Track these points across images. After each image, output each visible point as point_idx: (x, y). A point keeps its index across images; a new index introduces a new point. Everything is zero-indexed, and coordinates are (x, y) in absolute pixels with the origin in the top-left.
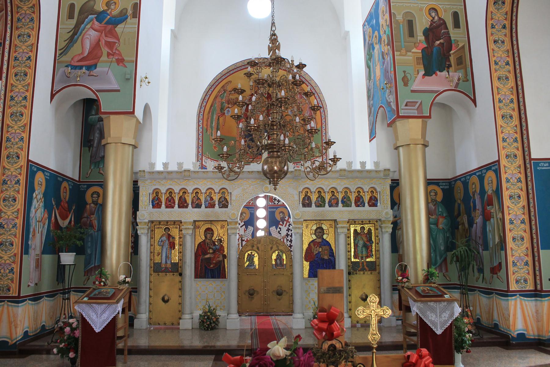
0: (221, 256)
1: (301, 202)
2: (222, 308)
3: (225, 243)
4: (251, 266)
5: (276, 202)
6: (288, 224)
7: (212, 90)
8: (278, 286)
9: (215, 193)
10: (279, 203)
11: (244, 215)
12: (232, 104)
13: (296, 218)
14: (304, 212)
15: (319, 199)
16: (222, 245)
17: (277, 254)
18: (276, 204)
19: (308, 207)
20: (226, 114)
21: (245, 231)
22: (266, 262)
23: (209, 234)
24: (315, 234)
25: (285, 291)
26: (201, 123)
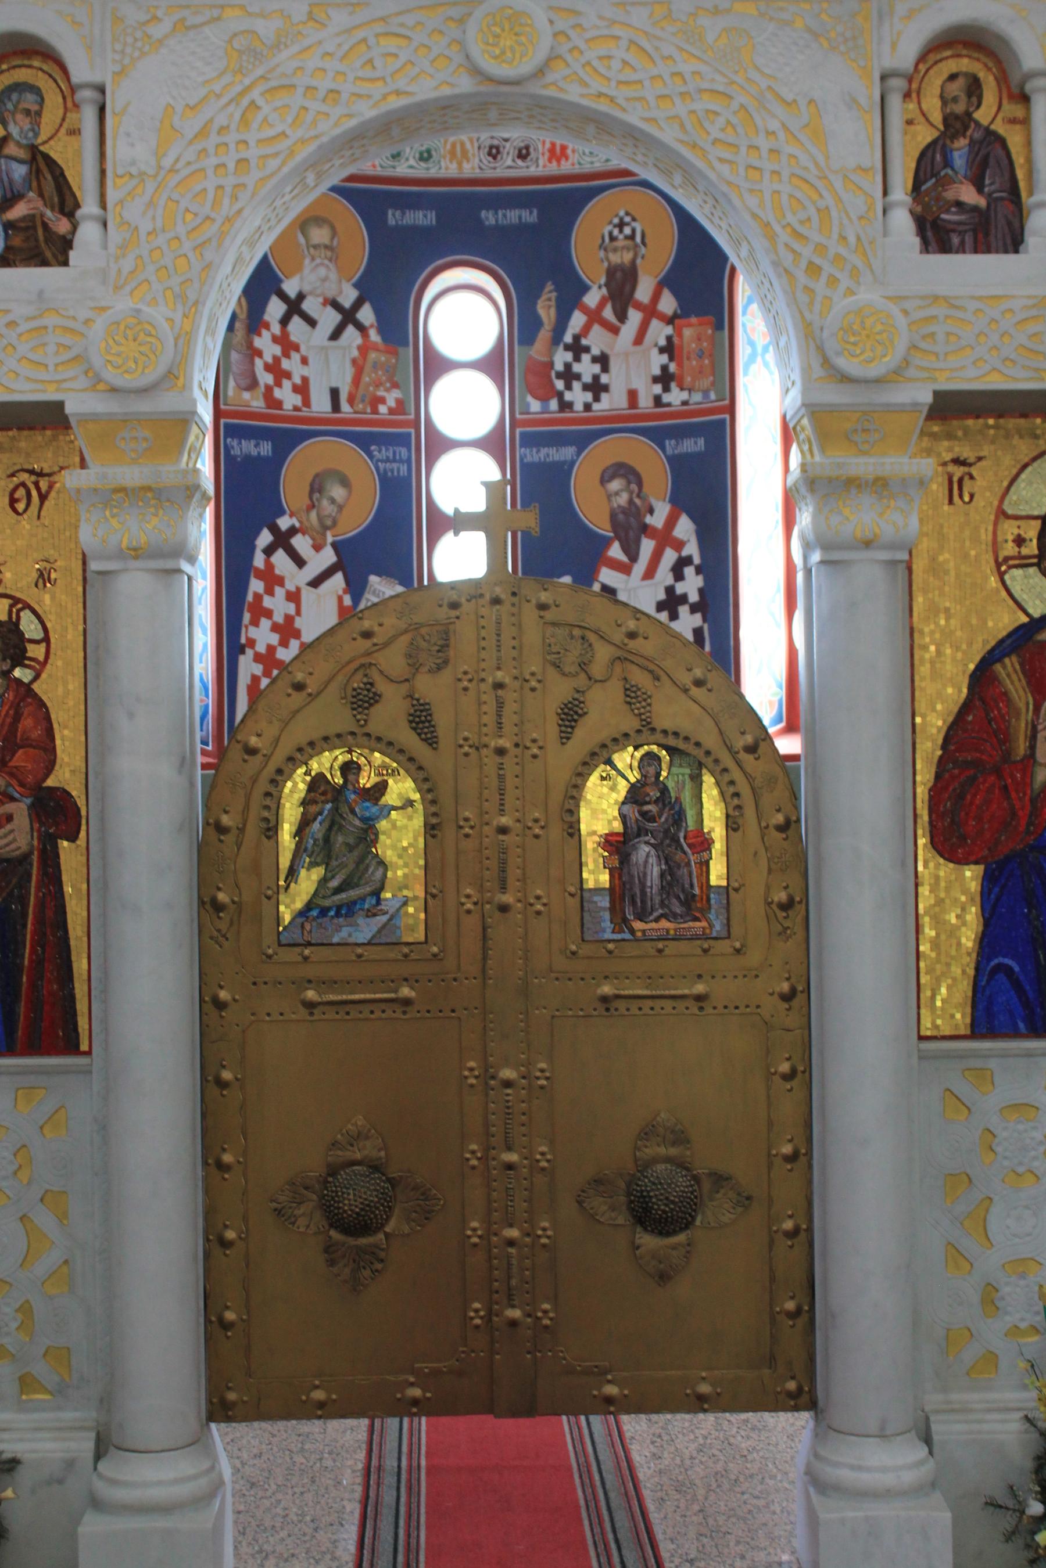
0: (20, 810)
1: (901, 193)
2: (40, 1369)
3: (56, 663)
4: (347, 911)
5: (578, 396)
6: (670, 557)
8: (648, 1132)
10: (597, 399)
11: (338, 492)
16: (26, 691)
17: (633, 776)
18: (579, 407)
19: (976, 251)
22: (513, 874)
25: (720, 1179)
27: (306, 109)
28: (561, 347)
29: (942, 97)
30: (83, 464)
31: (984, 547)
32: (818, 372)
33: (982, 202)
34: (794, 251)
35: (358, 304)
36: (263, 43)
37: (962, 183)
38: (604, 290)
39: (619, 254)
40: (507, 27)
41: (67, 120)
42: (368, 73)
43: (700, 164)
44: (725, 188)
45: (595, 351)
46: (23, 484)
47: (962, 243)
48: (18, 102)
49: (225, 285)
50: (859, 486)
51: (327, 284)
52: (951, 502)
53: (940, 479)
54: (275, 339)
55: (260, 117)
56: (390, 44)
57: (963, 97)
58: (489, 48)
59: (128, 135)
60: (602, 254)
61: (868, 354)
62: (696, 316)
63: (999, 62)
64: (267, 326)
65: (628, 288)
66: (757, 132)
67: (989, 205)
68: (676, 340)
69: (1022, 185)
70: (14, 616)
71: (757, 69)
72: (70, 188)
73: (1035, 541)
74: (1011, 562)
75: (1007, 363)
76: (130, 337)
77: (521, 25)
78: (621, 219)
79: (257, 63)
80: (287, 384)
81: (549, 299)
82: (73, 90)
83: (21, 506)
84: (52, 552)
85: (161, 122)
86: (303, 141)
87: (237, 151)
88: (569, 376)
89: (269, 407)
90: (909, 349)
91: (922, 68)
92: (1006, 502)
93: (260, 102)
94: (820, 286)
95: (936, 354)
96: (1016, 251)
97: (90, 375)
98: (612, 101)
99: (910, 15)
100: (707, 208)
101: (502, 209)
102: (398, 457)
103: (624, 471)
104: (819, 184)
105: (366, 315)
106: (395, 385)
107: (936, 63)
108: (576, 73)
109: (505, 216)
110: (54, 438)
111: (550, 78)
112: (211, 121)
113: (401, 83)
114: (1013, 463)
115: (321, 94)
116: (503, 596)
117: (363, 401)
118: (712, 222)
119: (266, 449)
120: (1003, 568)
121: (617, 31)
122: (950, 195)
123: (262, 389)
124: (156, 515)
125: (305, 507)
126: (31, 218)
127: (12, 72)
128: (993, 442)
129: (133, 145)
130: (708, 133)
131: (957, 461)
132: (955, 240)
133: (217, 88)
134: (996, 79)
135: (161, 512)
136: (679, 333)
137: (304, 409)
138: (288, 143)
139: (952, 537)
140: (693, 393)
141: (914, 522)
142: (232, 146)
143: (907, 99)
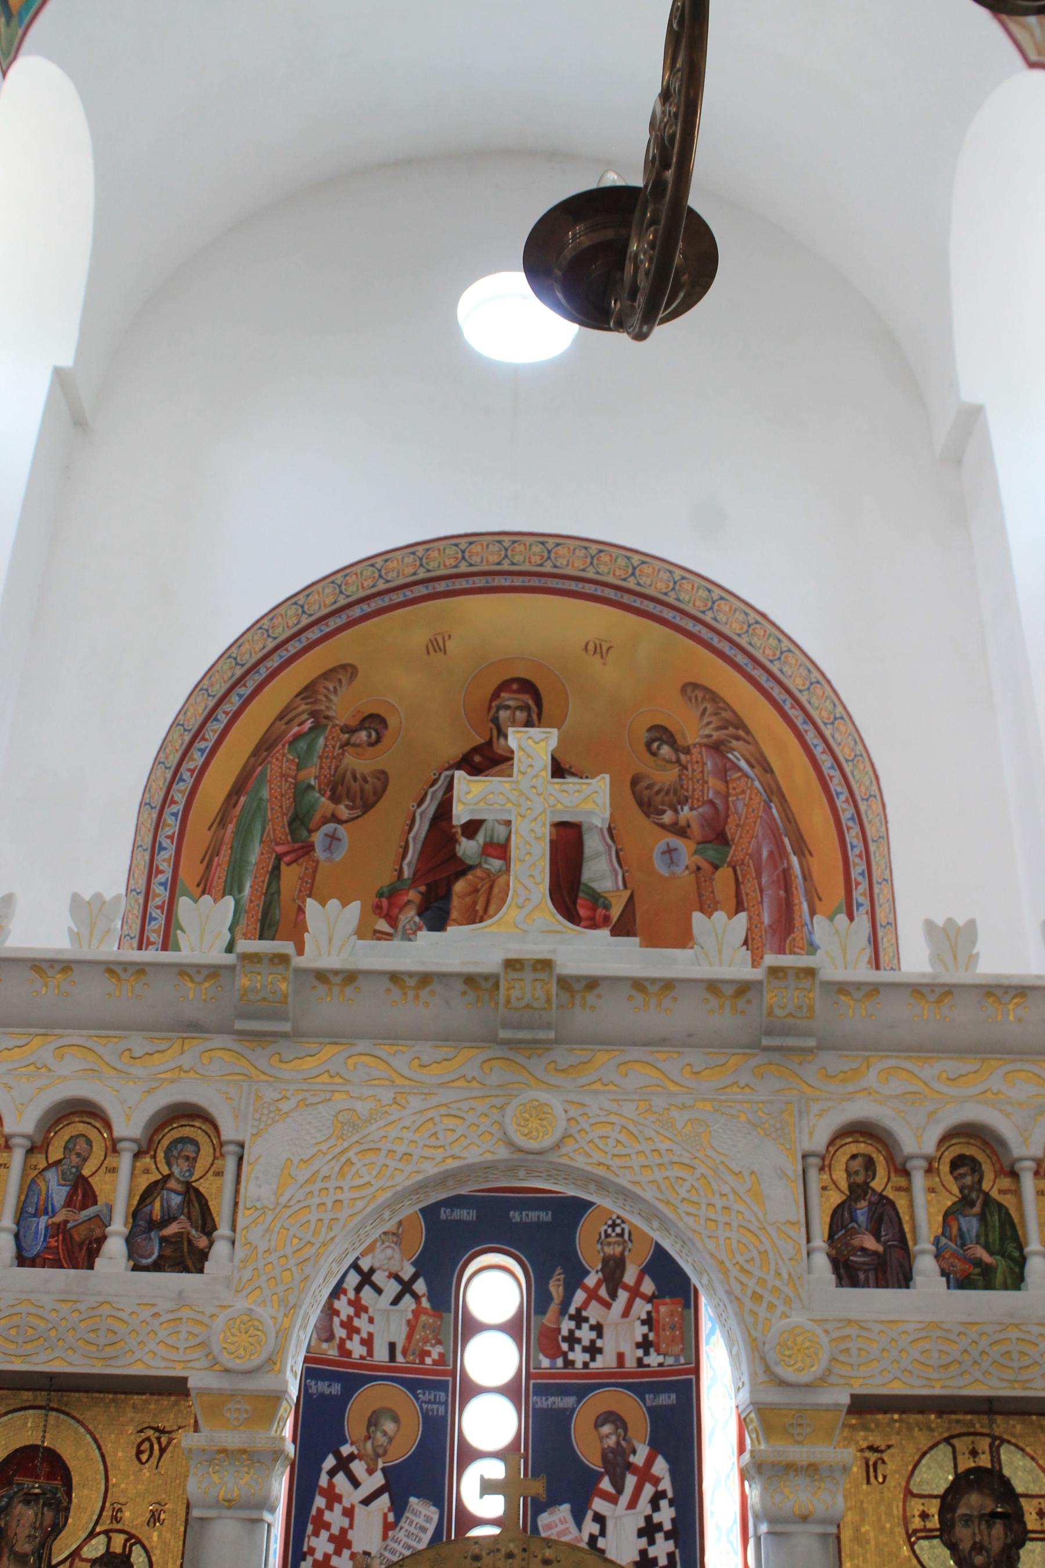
1: (820, 1241)
5: (579, 1356)
6: (648, 1490)
7: (245, 691)
9: (113, 1147)
10: (593, 1359)
11: (389, 1426)
12: (353, 800)
13: (786, 1373)
14: (852, 1331)
15: (971, 1224)
18: (579, 1364)
19: (877, 1286)
20: (319, 853)
21: (388, 1527)
23: (29, 1499)
24: (946, 1533)
26: (165, 855)
27: (387, 1166)
28: (567, 1317)
29: (847, 1171)
30: (196, 1430)
31: (896, 1520)
32: (762, 1377)
33: (880, 1249)
34: (742, 1283)
35: (414, 1278)
36: (360, 1118)
37: (864, 1234)
38: (600, 1275)
39: (612, 1247)
40: (534, 1114)
41: (214, 1166)
42: (432, 1142)
43: (671, 1216)
44: (690, 1234)
45: (593, 1321)
46: (148, 1439)
47: (867, 1279)
48: (182, 1150)
49: (317, 1292)
50: (796, 1470)
51: (392, 1261)
52: (868, 1482)
53: (859, 1463)
54: (350, 1303)
55: (354, 1169)
56: (450, 1122)
57: (862, 1173)
58: (522, 1129)
59: (257, 1178)
60: (599, 1247)
61: (799, 1365)
62: (670, 1297)
63: (886, 1146)
64: (345, 1292)
65: (618, 1273)
66: (713, 1193)
67: (885, 1250)
68: (654, 1314)
69: (909, 1236)
70: (127, 1549)
71: (713, 1148)
72: (211, 1214)
73: (936, 1517)
74: (919, 1534)
75: (906, 1373)
76: (243, 1331)
77: (544, 1113)
78: (614, 1221)
79: (354, 1132)
80: (356, 1338)
81: (559, 1280)
82: (221, 1145)
83: (144, 1457)
84: (163, 1496)
85: (282, 1170)
86: (382, 1189)
87: (335, 1194)
88: (572, 1340)
89: (341, 1356)
90: (831, 1361)
91: (832, 1149)
92: (912, 1483)
93: (354, 1159)
94: (762, 1311)
95: (851, 1365)
96: (907, 1287)
97: (210, 1357)
98: (608, 1169)
99: (822, 1113)
100: (678, 1247)
101: (526, 1210)
102: (437, 1400)
103: (611, 1417)
104: (759, 1233)
105: (420, 1286)
106: (439, 1342)
107: (842, 1146)
108: (582, 1148)
109: (527, 1215)
110: (176, 1403)
111: (564, 1150)
112: (317, 1171)
113: (456, 1150)
114: (915, 1451)
115: (398, 1156)
116: (516, 1551)
117: (413, 1354)
118: (681, 1256)
119: (336, 1389)
120: (913, 1539)
121: (612, 1118)
122: (856, 1242)
123: (337, 1341)
124: (248, 1473)
125: (363, 1438)
126: (179, 1235)
127: (180, 1129)
128: (898, 1433)
129: (260, 1187)
130: (678, 1194)
131: (872, 1448)
132: (862, 1276)
133: (324, 1147)
134: (885, 1158)
135: (252, 1471)
136: (656, 1308)
137: (368, 1358)
138: (372, 1190)
139: (870, 1511)
140: (667, 1357)
141: (840, 1501)
142: (331, 1190)
143: (822, 1172)
